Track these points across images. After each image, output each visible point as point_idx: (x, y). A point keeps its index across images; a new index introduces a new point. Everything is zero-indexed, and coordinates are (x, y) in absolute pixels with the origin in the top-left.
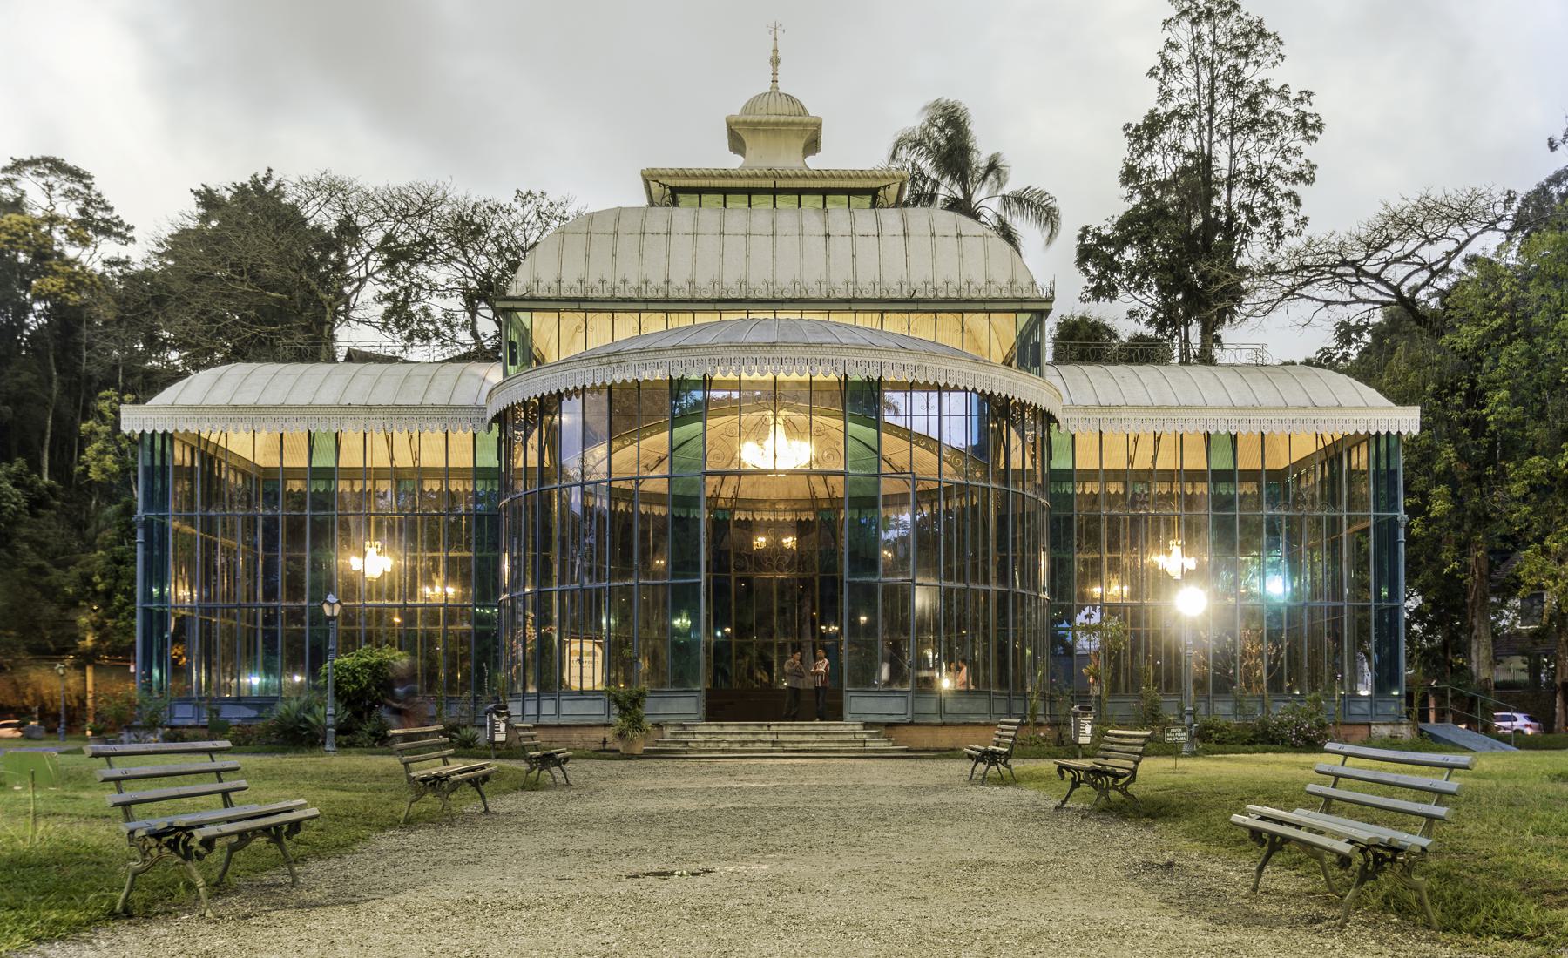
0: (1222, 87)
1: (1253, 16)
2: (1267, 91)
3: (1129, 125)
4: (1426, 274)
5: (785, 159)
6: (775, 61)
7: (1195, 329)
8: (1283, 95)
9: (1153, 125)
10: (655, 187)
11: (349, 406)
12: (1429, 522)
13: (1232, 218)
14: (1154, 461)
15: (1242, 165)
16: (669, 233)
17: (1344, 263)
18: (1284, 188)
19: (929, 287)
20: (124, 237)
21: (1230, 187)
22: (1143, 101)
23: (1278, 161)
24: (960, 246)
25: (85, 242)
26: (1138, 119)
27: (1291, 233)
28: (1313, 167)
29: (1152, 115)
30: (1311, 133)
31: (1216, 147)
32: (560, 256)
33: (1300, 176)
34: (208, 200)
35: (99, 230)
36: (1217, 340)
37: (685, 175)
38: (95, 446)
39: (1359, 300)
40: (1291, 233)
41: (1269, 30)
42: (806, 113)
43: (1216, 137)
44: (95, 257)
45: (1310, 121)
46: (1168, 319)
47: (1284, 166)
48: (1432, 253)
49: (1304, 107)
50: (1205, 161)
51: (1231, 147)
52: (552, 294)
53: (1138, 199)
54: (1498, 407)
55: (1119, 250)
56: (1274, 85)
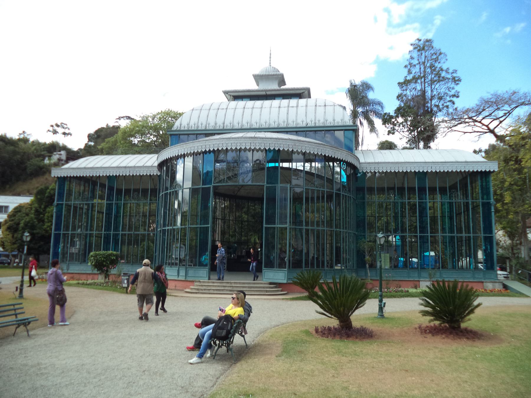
0: (429, 70)
1: (438, 48)
5: (273, 86)
8: (447, 71)
12: (504, 204)
13: (432, 110)
14: (307, 102)
15: (435, 93)
21: (431, 100)
23: (447, 91)
26: (402, 80)
28: (459, 92)
30: (457, 82)
31: (426, 89)
33: (454, 96)
39: (475, 132)
41: (442, 51)
42: (278, 71)
43: (426, 85)
45: (456, 79)
47: (448, 92)
49: (454, 75)
50: (424, 92)
51: (431, 88)
56: (445, 68)
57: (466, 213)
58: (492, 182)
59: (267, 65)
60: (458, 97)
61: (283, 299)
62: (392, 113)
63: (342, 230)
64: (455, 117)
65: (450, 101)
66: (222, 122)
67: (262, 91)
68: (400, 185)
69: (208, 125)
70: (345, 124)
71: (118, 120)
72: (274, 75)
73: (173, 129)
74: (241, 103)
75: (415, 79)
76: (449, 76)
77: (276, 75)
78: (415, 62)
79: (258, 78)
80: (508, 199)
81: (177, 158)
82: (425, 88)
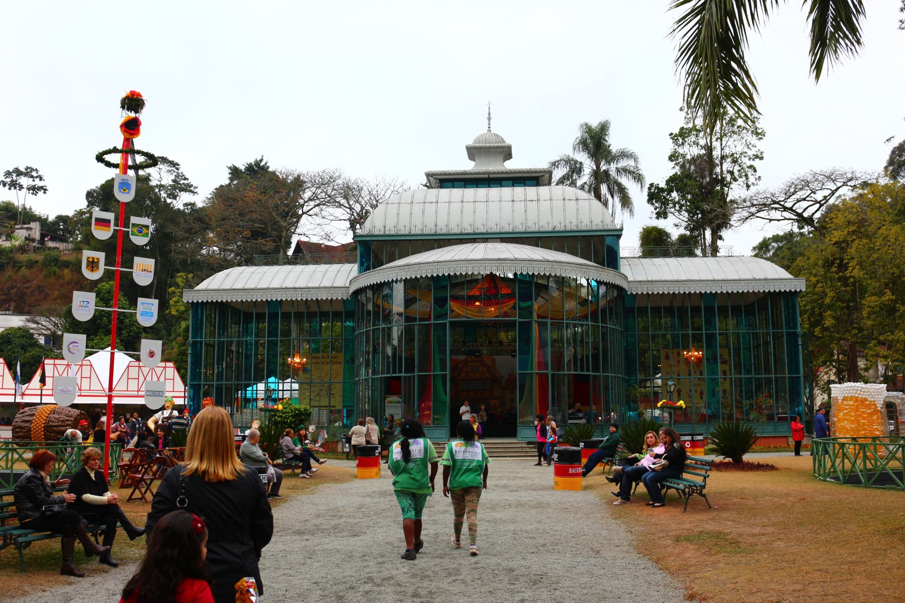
3: (671, 134)
4: (818, 205)
6: (489, 119)
7: (708, 233)
11: (286, 288)
13: (723, 179)
17: (775, 203)
18: (749, 163)
20: (193, 192)
23: (746, 150)
24: (577, 204)
25: (175, 197)
26: (676, 131)
27: (753, 184)
29: (682, 129)
32: (385, 215)
33: (757, 157)
34: (235, 172)
35: (182, 190)
36: (720, 238)
37: (446, 174)
38: (174, 299)
39: (785, 219)
40: (753, 184)
42: (504, 141)
43: (714, 139)
44: (181, 202)
46: (696, 227)
48: (819, 196)
50: (709, 149)
52: (382, 233)
53: (678, 168)
54: (855, 272)
55: (669, 194)
58: (801, 302)
59: (485, 130)
60: (761, 158)
62: (663, 185)
63: (601, 374)
64: (755, 203)
67: (484, 173)
70: (606, 228)
72: (497, 147)
77: (501, 147)
79: (473, 152)
80: (829, 322)
82: (711, 143)
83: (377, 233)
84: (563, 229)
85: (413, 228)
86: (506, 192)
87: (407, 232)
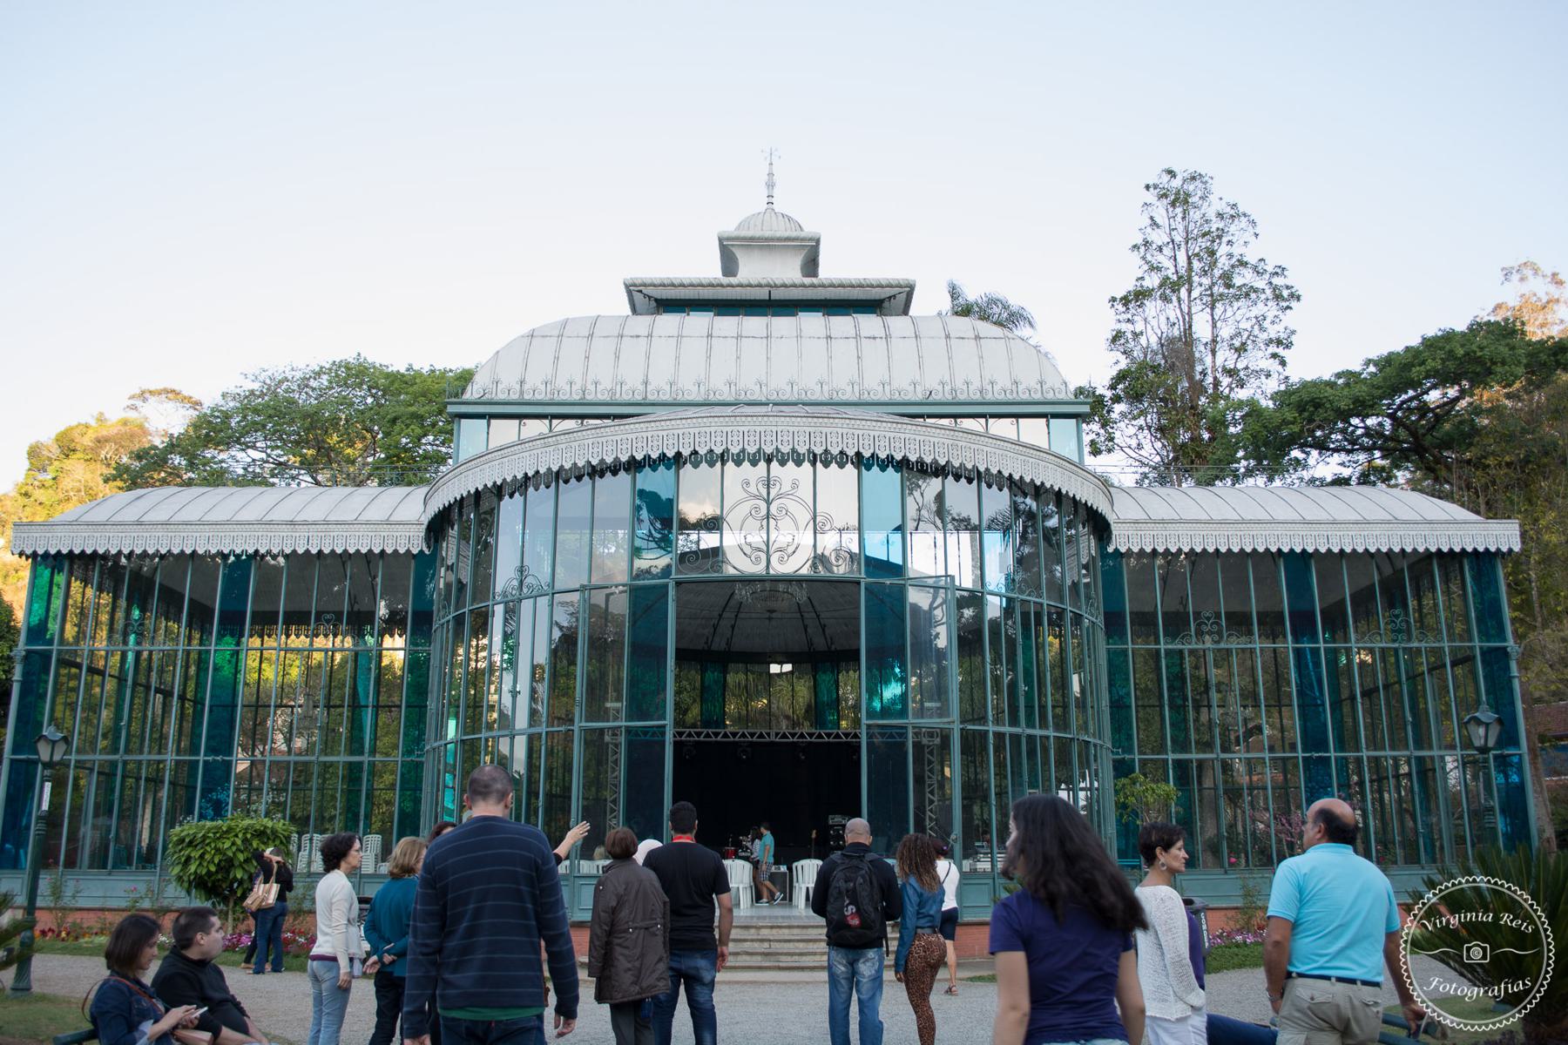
2: (1243, 264)
5: (784, 272)
9: (1139, 296)
10: (638, 297)
16: (650, 336)
19: (947, 388)
22: (1128, 274)
24: (979, 347)
28: (1293, 332)
33: (1279, 342)
45: (1285, 293)
49: (1277, 281)
52: (514, 397)
57: (1345, 694)
61: (971, 979)
65: (1274, 356)
66: (641, 378)
68: (1174, 606)
69: (591, 387)
71: (139, 403)
73: (467, 396)
74: (669, 321)
75: (1171, 287)
76: (1260, 283)
78: (1159, 237)
81: (498, 491)
83: (502, 397)
84: (949, 398)
85: (591, 387)
86: (812, 322)
87: (576, 397)
